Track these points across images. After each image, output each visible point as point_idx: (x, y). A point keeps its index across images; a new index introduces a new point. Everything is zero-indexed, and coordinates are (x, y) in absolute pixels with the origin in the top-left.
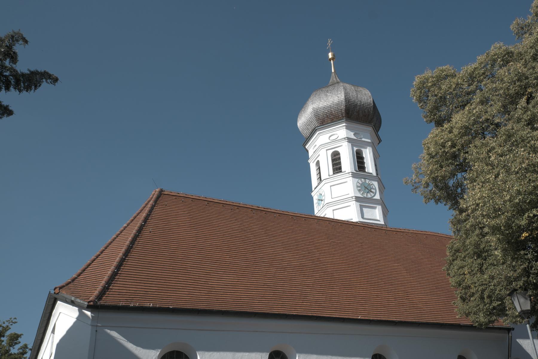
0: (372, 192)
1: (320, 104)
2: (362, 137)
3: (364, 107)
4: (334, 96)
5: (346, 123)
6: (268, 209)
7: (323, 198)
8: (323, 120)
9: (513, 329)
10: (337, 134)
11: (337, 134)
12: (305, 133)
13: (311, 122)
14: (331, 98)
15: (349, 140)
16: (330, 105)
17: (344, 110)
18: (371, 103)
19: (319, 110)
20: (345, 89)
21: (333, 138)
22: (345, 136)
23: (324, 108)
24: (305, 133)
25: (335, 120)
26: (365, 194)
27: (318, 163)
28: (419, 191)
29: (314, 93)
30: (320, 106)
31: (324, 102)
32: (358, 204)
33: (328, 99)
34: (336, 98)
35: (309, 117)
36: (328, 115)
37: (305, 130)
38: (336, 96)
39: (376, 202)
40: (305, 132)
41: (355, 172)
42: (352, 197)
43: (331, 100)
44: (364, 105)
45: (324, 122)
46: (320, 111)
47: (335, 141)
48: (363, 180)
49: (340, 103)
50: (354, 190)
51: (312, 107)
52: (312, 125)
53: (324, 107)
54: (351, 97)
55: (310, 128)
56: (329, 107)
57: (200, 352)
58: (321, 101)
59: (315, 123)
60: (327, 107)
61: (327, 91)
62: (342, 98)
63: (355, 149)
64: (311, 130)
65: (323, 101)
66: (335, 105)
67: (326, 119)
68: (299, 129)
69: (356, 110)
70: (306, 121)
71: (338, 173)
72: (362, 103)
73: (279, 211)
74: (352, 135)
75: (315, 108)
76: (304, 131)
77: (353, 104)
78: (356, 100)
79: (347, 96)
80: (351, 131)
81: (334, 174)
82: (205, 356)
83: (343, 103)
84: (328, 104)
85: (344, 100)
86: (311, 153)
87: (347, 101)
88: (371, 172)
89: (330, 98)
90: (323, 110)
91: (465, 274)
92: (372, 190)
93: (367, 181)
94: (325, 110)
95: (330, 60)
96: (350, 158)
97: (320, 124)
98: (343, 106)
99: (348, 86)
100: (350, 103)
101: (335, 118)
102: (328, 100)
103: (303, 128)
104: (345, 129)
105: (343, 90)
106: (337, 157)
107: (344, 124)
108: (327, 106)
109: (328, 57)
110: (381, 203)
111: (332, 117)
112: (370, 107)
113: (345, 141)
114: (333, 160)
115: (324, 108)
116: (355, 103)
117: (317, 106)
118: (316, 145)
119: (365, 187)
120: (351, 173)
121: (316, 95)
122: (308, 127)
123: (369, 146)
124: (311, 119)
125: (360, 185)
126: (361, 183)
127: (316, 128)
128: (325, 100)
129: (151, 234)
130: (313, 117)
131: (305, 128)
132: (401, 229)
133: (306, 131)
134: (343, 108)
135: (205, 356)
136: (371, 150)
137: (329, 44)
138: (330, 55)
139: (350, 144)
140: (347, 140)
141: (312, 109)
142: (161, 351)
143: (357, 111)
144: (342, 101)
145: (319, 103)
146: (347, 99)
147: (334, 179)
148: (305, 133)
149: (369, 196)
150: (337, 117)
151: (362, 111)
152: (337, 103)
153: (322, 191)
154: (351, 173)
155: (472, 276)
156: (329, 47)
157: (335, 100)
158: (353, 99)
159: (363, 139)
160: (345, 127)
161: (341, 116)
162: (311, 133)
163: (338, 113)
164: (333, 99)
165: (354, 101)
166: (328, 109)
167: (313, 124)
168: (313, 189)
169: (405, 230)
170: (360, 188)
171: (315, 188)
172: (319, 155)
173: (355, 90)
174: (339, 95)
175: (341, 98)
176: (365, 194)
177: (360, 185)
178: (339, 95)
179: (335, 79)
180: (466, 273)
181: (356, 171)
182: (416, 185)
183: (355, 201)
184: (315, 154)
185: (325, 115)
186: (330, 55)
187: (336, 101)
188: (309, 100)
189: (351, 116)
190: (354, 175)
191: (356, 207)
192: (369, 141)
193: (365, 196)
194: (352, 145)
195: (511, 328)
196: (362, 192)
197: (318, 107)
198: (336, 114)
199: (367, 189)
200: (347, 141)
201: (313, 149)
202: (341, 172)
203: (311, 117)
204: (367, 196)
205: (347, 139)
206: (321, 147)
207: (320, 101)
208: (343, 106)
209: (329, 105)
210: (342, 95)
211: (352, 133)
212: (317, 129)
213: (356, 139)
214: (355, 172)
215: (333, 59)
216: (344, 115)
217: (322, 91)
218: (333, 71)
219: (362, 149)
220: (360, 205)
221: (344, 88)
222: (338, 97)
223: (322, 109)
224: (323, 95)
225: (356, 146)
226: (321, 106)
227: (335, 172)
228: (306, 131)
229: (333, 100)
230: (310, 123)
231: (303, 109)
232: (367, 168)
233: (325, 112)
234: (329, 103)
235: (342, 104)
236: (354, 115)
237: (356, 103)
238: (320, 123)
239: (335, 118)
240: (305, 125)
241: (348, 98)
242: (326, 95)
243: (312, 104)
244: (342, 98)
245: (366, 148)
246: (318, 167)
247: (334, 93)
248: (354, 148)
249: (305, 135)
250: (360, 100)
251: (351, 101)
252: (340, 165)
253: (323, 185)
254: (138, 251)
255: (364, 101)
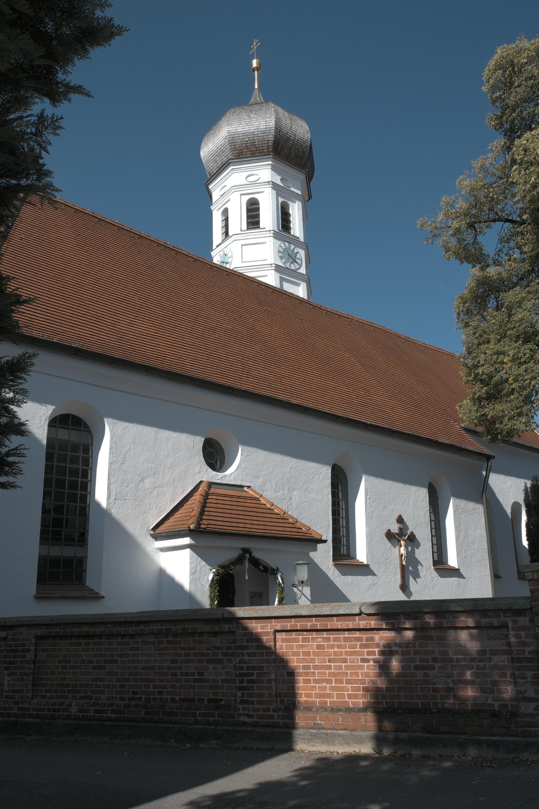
0: (296, 262)
1: (239, 128)
2: (291, 185)
3: (299, 144)
4: (260, 119)
5: (272, 161)
6: (178, 249)
7: (230, 260)
8: (240, 151)
9: (494, 457)
10: (258, 175)
11: (258, 175)
12: (210, 166)
13: (222, 152)
14: (256, 121)
15: (275, 186)
16: (253, 131)
17: (272, 142)
18: (308, 140)
19: (236, 136)
20: (277, 114)
21: (251, 179)
22: (270, 180)
23: (245, 134)
24: (210, 167)
25: (256, 154)
26: (288, 263)
27: (225, 212)
28: (439, 242)
29: (232, 110)
30: (238, 130)
31: (245, 125)
32: (278, 275)
33: (252, 122)
34: (263, 122)
35: (221, 143)
36: (248, 145)
37: (211, 162)
38: (264, 120)
39: (300, 277)
40: (211, 165)
41: (278, 231)
42: (271, 264)
43: (255, 124)
44: (299, 142)
45: (242, 155)
46: (238, 138)
47: (254, 183)
48: (287, 244)
49: (268, 131)
50: (274, 256)
51: (228, 130)
52: (224, 157)
53: (244, 132)
54: (284, 126)
55: (220, 160)
56: (252, 134)
57: (110, 420)
58: (242, 123)
59: (228, 154)
60: (249, 134)
61: (251, 111)
62: (271, 124)
63: (281, 200)
64: (220, 164)
65: (244, 123)
66: (261, 132)
67: (245, 150)
68: (202, 159)
69: (288, 145)
70: (215, 149)
71: (254, 228)
72: (297, 138)
73: (193, 255)
74: (278, 180)
75: (232, 131)
76: (210, 163)
77: (285, 136)
78: (289, 132)
79: (278, 123)
80: (278, 175)
81: (248, 229)
82: (116, 428)
83: (273, 131)
84: (250, 129)
85: (274, 128)
86: (216, 196)
87: (278, 130)
88: (298, 236)
89: (254, 122)
90: (243, 137)
91: (503, 363)
92: (297, 260)
93: (292, 247)
94: (245, 137)
95: (254, 70)
96: (272, 211)
97: (236, 156)
98: (271, 136)
99: (281, 111)
100: (281, 134)
101: (258, 151)
102: (251, 124)
103: (208, 159)
104: (270, 170)
105: (273, 113)
106: (255, 206)
107: (270, 162)
108: (249, 131)
109: (252, 65)
110: (306, 280)
111: (254, 149)
112: (306, 146)
113: (269, 186)
114: (248, 211)
115: (245, 134)
116: (287, 135)
117: (234, 129)
118: (225, 186)
119: (289, 254)
120: (272, 232)
121: (234, 113)
122: (216, 158)
123: (299, 200)
124: (223, 147)
125: (282, 250)
126: (284, 248)
127: (230, 161)
128: (247, 122)
129: (22, 241)
130: (227, 144)
131: (211, 160)
132: (343, 314)
133: (213, 164)
134: (270, 139)
135: (116, 428)
136: (301, 206)
137: (254, 47)
138: (255, 63)
139: (275, 192)
140: (271, 186)
141: (226, 133)
142: (54, 410)
143: (289, 147)
144: (271, 129)
145: (238, 126)
146: (277, 128)
147: (248, 236)
148: (210, 167)
149: (293, 267)
150: (260, 151)
151: (295, 149)
152: (264, 130)
153: (228, 250)
154: (272, 232)
155: (516, 365)
156: (254, 52)
157: (261, 125)
158: (285, 129)
159: (292, 189)
160: (270, 167)
161: (266, 150)
162: (219, 167)
163: (263, 145)
164: (259, 123)
165: (287, 133)
166: (249, 136)
167: (225, 156)
168: (214, 247)
169: (348, 315)
170: (282, 255)
171: (218, 246)
172: (229, 200)
173: (289, 117)
174: (268, 120)
175: (270, 124)
176: (288, 263)
177: (282, 250)
178: (268, 120)
179: (259, 99)
180: (505, 361)
181: (279, 230)
182: (436, 232)
183: (274, 271)
184: (221, 199)
185: (244, 145)
186: (255, 63)
187: (262, 127)
188: (223, 119)
189: (280, 152)
190: (276, 236)
191: (275, 279)
192: (300, 193)
193: (288, 266)
194: (277, 193)
195: (491, 456)
196: (285, 260)
197: (235, 131)
198: (260, 146)
199: (292, 258)
200: (271, 187)
201: (221, 190)
202: (259, 228)
203: (224, 144)
204: (290, 267)
205: (272, 184)
206: (234, 189)
207: (239, 123)
208: (271, 136)
209: (251, 131)
210: (272, 119)
211: (279, 178)
212: (230, 163)
213: (283, 186)
214: (278, 231)
215: (258, 69)
216: (271, 150)
217: (243, 109)
218: (256, 87)
219: (289, 202)
220: (280, 277)
221: (275, 111)
222: (266, 121)
223: (241, 135)
224: (244, 115)
225: (282, 197)
226: (240, 130)
227: (249, 227)
228: (213, 164)
229: (258, 125)
230: (221, 153)
231: (212, 132)
232: (293, 229)
233: (245, 140)
234: (253, 128)
235: (271, 134)
236: (284, 153)
237: (289, 136)
238: (235, 154)
239: (258, 151)
240: (212, 155)
241: (279, 126)
242: (249, 116)
243: (227, 125)
244: (271, 124)
245: (295, 202)
246: (224, 218)
247: (260, 115)
248: (279, 198)
249: (210, 169)
250: (295, 132)
251: (283, 131)
252: (258, 218)
253: (232, 242)
254: (8, 259)
255: (299, 135)
